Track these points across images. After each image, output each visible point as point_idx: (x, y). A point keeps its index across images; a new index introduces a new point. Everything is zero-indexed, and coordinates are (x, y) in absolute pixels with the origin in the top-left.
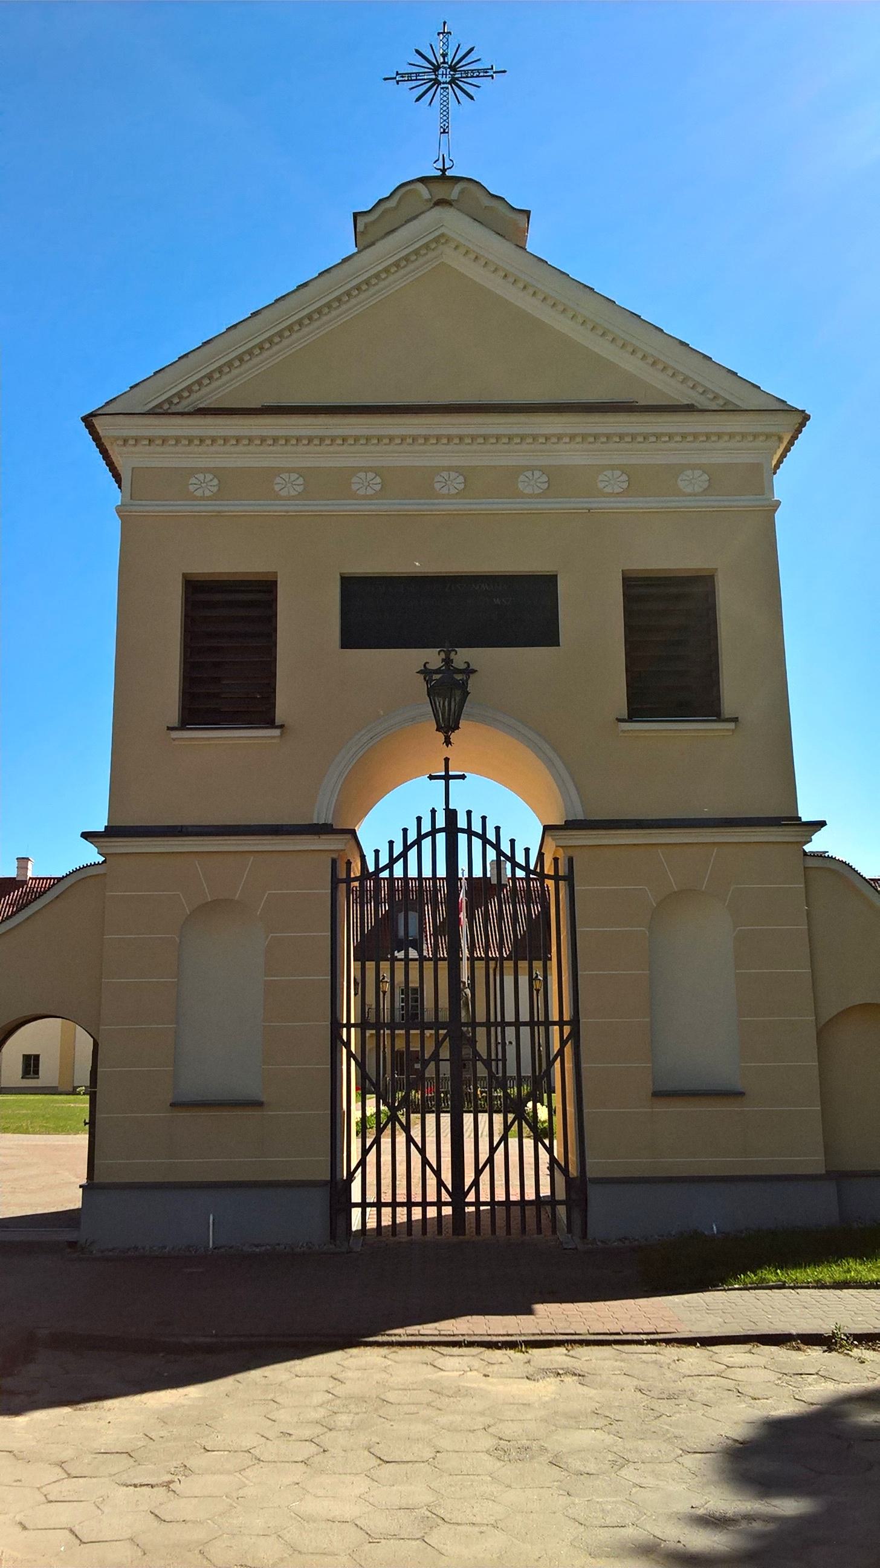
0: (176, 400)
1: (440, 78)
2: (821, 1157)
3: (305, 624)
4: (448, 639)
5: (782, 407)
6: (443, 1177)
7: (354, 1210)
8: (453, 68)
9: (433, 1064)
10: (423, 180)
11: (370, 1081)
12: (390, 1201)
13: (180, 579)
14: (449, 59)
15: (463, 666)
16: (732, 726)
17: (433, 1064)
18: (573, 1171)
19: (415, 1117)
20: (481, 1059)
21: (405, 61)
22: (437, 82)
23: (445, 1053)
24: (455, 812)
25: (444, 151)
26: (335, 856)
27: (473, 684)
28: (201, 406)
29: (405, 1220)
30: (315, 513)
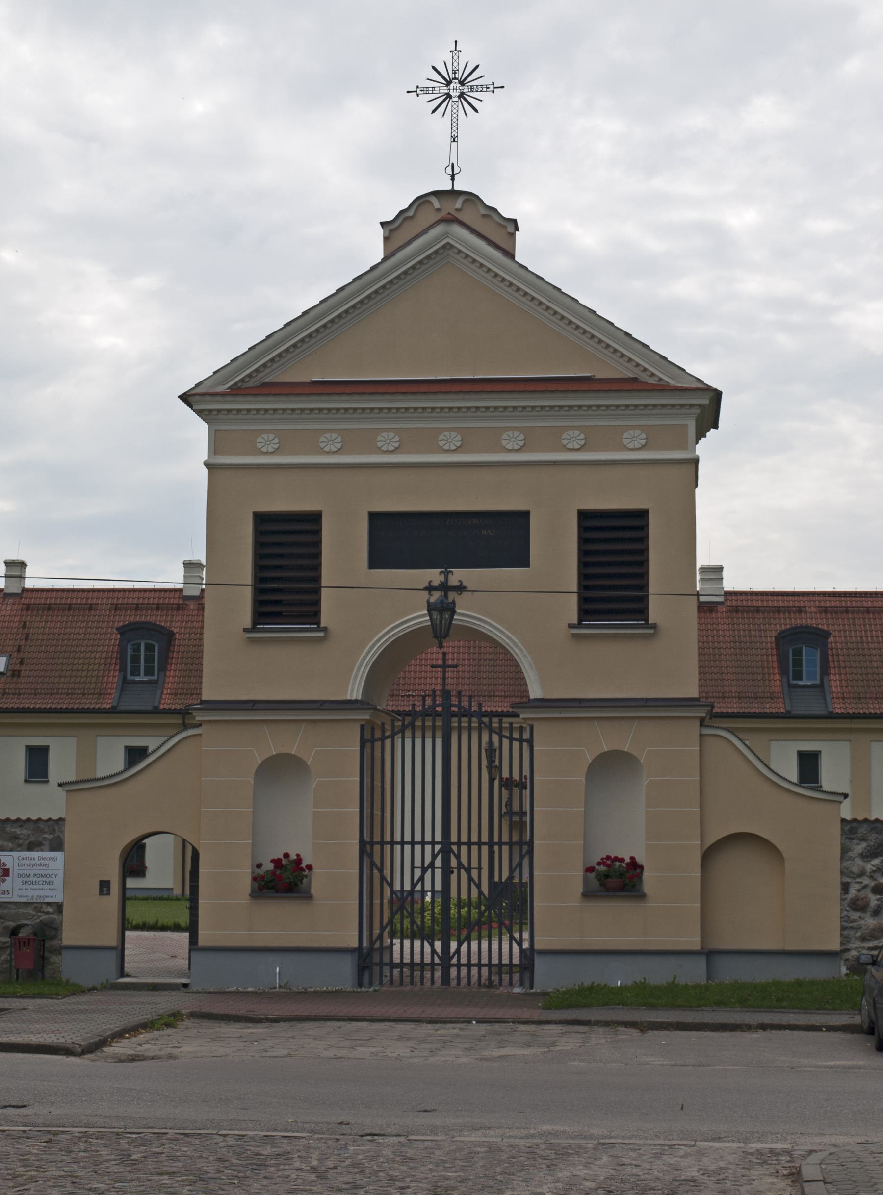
0: (247, 379)
1: (451, 93)
2: (698, 939)
3: (343, 552)
4: (447, 561)
5: (699, 385)
6: (466, 876)
7: (518, 962)
8: (462, 83)
9: (430, 870)
10: (435, 193)
11: (387, 882)
12: (187, 934)
13: (251, 515)
14: (458, 76)
15: (457, 584)
16: (652, 631)
17: (430, 870)
18: (526, 945)
19: (428, 960)
20: (464, 867)
21: (424, 76)
22: (449, 96)
23: (438, 862)
24: (449, 692)
25: (454, 160)
26: (363, 723)
27: (464, 584)
28: (266, 381)
29: (472, 942)
30: (350, 472)
